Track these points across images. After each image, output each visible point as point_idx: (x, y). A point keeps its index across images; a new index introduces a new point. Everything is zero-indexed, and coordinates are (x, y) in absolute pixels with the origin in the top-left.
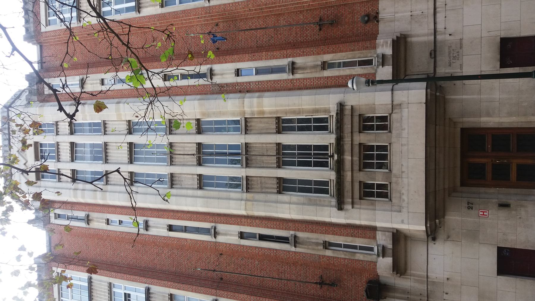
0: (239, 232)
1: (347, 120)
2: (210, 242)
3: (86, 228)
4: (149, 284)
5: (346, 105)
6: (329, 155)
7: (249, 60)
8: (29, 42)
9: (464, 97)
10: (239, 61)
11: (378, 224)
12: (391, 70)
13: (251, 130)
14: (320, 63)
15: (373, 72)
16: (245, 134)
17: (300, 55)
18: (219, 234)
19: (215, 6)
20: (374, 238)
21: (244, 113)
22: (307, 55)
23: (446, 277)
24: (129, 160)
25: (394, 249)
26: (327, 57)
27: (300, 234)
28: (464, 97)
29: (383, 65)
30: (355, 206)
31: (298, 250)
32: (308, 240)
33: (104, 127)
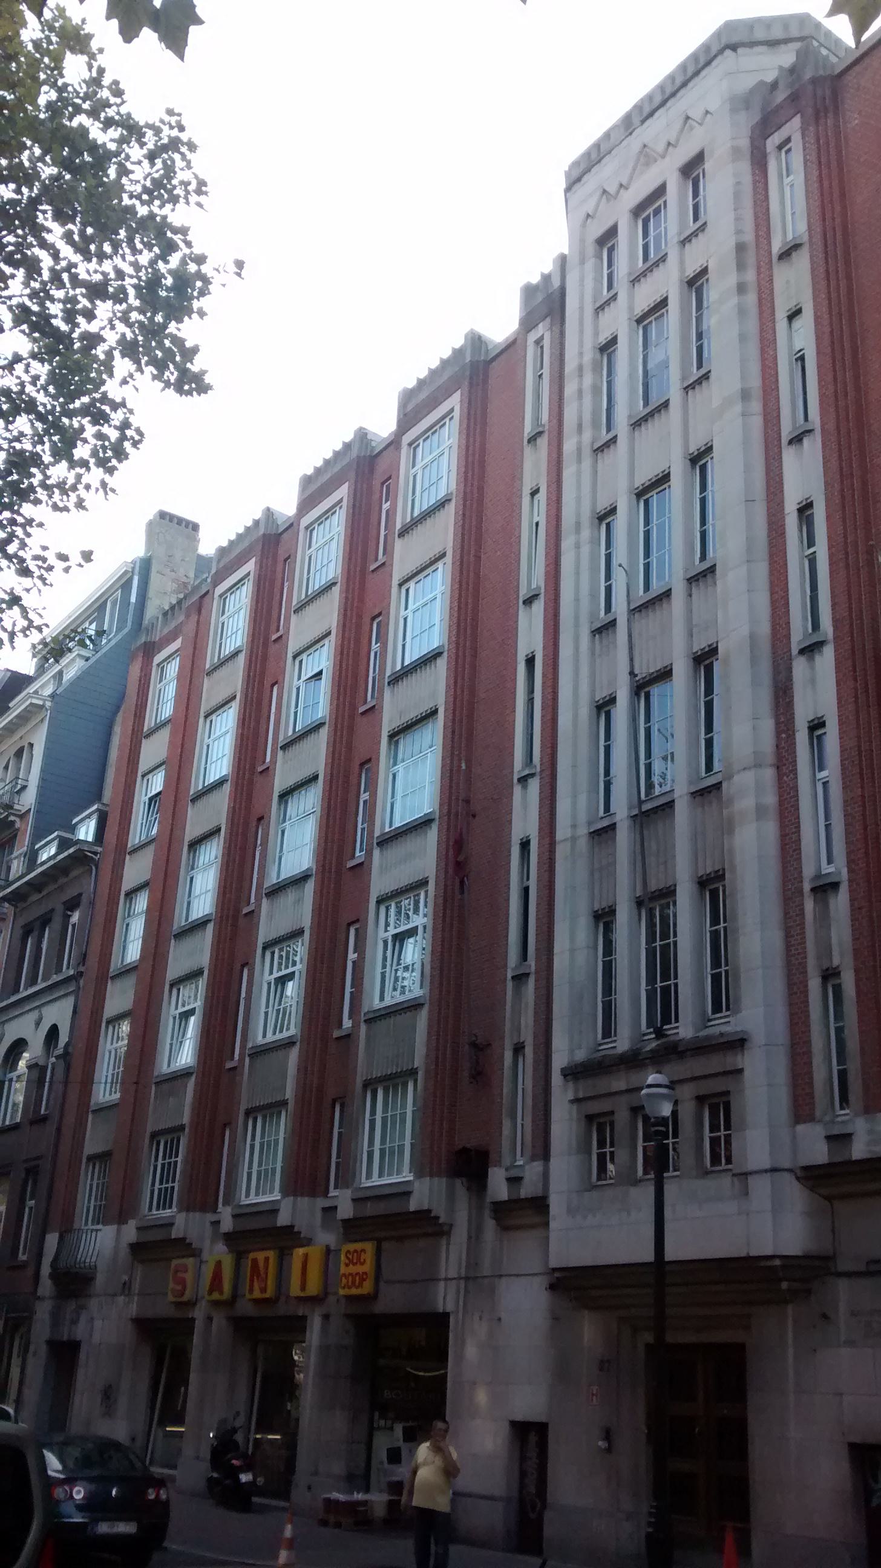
0: (823, 716)
1: (713, 1063)
2: (512, 772)
3: (770, 253)
4: (823, 430)
5: (743, 1055)
6: (665, 1027)
7: (843, 750)
8: (466, 336)
9: (791, 1351)
10: (841, 723)
11: (554, 1162)
12: (503, 1199)
13: (703, 806)
14: (836, 962)
15: (818, 1113)
16: (692, 793)
17: (852, 900)
18: (811, 659)
19: (512, 794)
20: (533, 1158)
21: (730, 777)
22: (854, 919)
23: (503, 1315)
24: (641, 488)
25: (518, 1201)
26: (848, 980)
27: (531, 982)
28: (791, 1351)
29: (829, 1138)
30: (575, 1107)
31: (510, 985)
32: (523, 1005)
33: (699, 378)
